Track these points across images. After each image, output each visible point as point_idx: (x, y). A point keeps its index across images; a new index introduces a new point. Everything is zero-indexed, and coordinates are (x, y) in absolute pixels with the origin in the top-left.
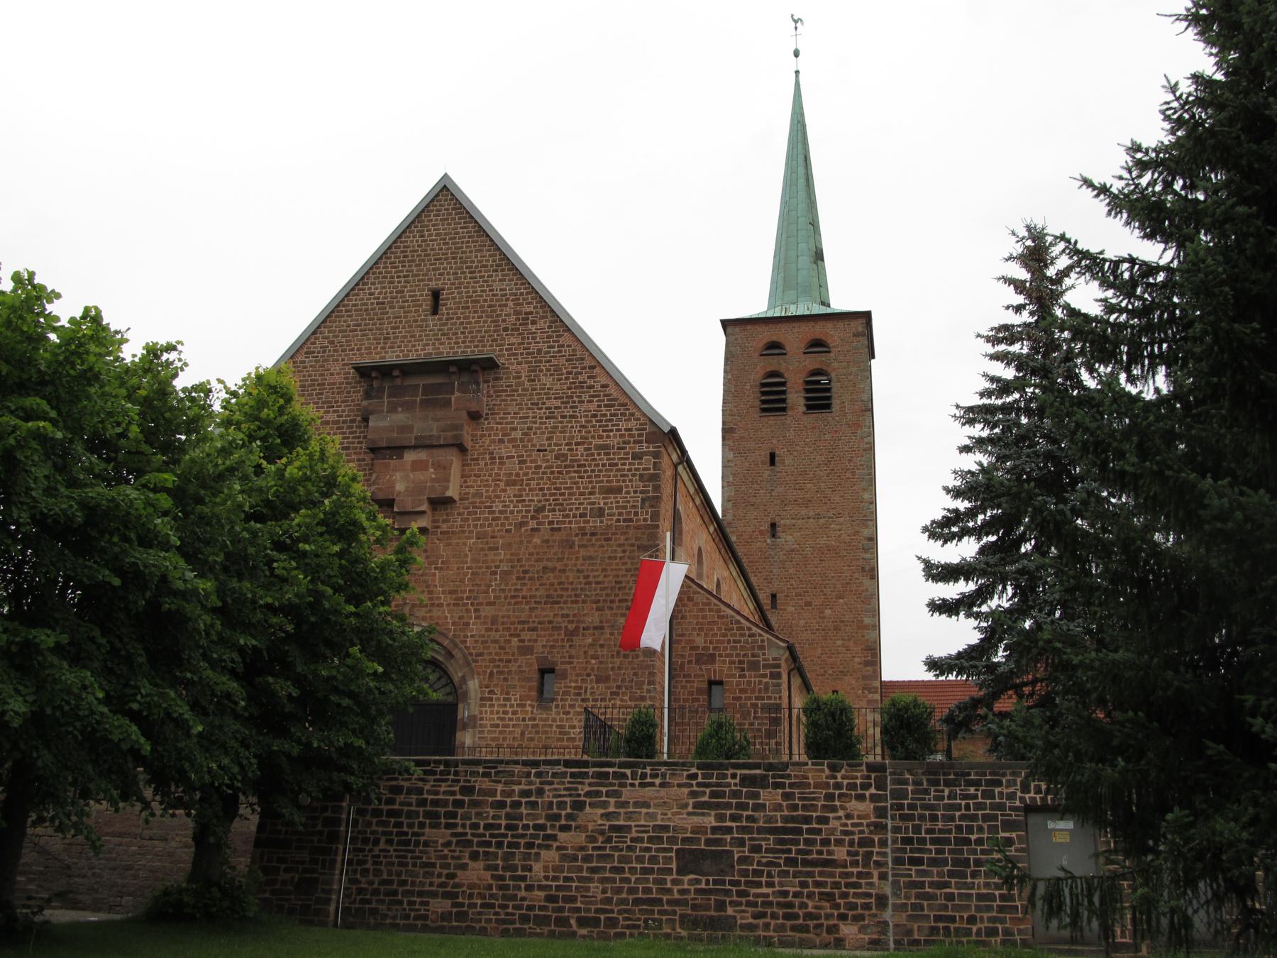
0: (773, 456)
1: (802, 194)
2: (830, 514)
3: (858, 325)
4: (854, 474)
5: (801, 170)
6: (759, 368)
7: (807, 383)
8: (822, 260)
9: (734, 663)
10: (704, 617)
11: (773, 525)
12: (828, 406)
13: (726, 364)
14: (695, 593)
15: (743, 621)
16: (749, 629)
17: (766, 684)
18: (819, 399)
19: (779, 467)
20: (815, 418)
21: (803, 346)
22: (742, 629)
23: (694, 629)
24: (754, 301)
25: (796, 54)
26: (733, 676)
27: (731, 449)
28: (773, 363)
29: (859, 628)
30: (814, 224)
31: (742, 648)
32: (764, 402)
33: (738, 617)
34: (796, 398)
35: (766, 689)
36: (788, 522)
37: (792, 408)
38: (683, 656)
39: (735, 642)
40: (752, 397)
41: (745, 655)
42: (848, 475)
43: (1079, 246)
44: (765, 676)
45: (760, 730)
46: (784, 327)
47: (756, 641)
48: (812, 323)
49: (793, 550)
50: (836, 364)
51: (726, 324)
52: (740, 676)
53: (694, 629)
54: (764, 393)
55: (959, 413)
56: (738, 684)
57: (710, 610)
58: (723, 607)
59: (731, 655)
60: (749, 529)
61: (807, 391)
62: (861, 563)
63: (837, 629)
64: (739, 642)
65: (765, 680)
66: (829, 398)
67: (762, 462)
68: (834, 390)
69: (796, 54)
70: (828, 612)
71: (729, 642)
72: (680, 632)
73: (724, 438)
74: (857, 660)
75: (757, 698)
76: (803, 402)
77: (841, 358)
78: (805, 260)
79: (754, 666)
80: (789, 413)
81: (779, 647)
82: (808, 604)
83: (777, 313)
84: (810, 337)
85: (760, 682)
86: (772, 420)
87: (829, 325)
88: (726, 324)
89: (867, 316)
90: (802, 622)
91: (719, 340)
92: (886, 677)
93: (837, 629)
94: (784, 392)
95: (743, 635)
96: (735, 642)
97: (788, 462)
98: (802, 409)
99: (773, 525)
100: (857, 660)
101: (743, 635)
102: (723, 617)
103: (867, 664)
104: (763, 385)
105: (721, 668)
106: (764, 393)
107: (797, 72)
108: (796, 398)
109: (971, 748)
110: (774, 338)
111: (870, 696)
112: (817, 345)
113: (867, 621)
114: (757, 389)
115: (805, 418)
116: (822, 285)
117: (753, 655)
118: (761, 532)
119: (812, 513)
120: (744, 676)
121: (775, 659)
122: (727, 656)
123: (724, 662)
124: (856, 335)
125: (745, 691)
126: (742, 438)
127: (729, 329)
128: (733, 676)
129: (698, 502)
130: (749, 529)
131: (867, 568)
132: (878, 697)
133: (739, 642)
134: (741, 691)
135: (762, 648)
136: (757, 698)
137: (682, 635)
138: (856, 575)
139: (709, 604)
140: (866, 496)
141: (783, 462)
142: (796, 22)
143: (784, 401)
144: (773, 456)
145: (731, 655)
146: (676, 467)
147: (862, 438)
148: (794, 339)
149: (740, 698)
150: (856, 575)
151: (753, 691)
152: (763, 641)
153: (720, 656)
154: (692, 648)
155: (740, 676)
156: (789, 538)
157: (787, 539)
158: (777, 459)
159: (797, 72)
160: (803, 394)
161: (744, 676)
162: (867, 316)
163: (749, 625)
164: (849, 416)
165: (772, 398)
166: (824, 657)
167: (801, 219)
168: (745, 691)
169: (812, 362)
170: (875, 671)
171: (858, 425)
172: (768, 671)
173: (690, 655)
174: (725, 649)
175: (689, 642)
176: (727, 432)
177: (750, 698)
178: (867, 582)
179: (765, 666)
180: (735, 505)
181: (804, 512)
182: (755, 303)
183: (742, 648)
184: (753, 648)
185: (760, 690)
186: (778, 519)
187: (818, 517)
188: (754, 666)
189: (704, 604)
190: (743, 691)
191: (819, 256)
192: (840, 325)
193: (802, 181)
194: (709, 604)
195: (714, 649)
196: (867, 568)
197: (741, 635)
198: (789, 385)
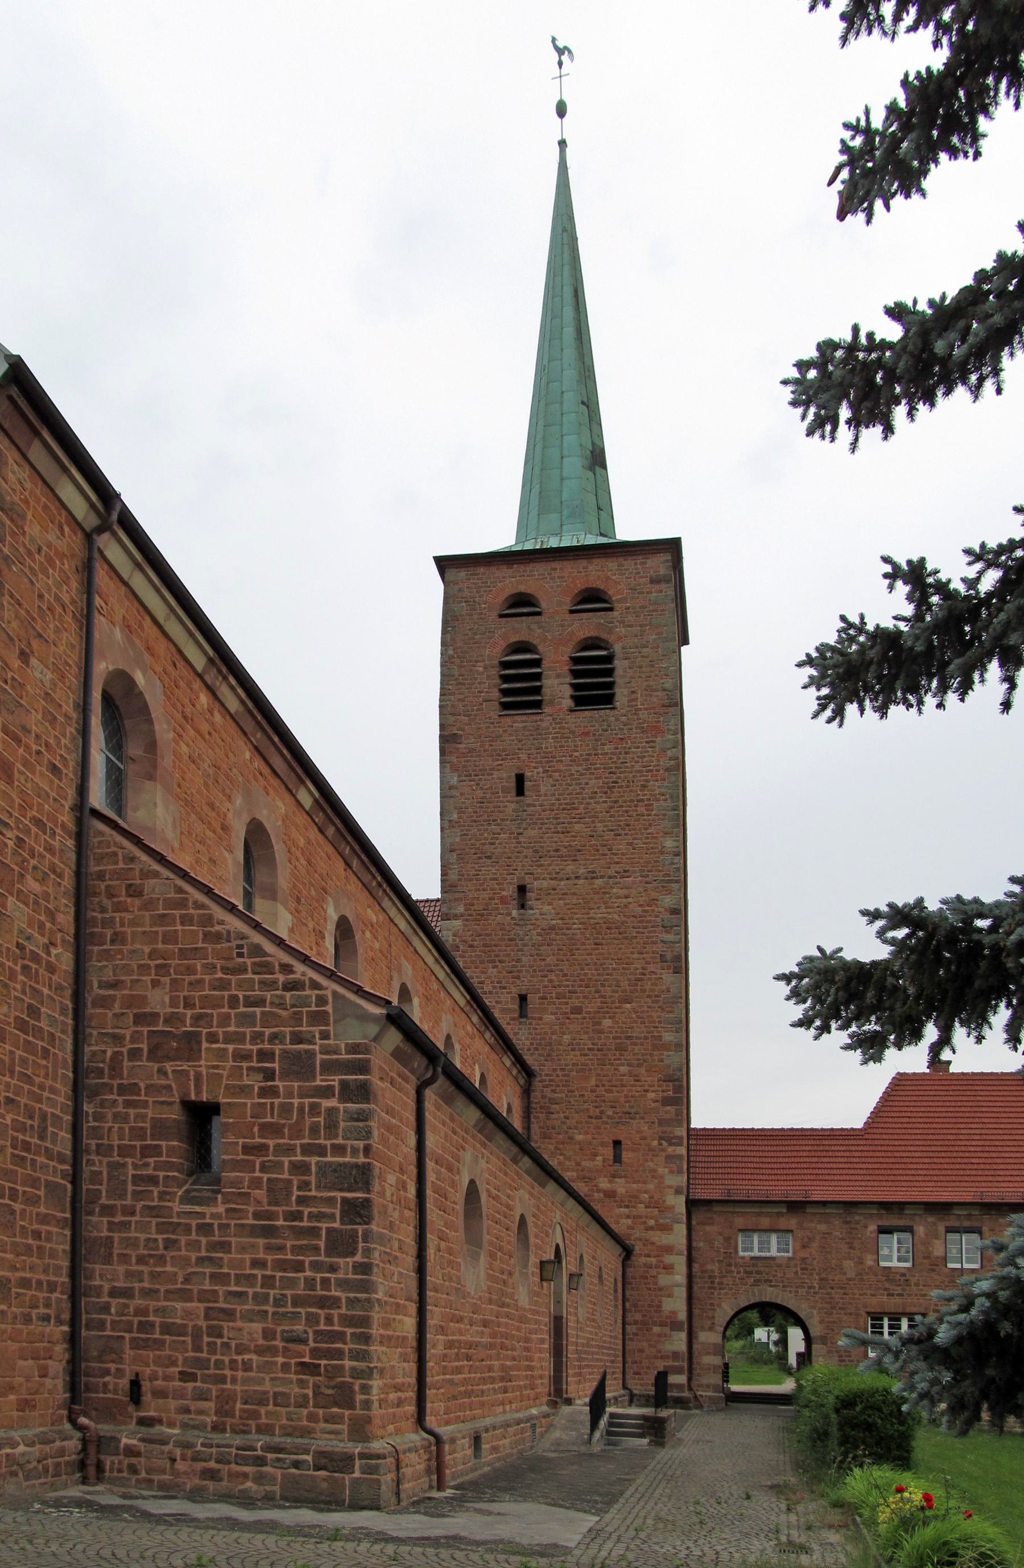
0: (520, 779)
1: (570, 353)
2: (610, 872)
3: (659, 564)
4: (649, 807)
5: (569, 312)
6: (498, 637)
7: (576, 661)
8: (604, 466)
9: (246, 1057)
10: (170, 938)
11: (522, 889)
12: (608, 700)
13: (444, 632)
14: (147, 874)
15: (269, 947)
16: (286, 968)
17: (331, 1112)
18: (594, 683)
19: (530, 796)
20: (591, 717)
21: (568, 600)
22: (265, 967)
23: (144, 969)
24: (494, 526)
25: (561, 110)
26: (244, 1090)
27: (455, 769)
28: (521, 629)
29: (655, 1047)
30: (590, 406)
31: (267, 1019)
32: (505, 692)
33: (257, 938)
34: (557, 686)
35: (331, 1127)
36: (545, 884)
37: (551, 703)
38: (117, 1039)
39: (249, 1002)
40: (488, 685)
41: (274, 1037)
42: (641, 809)
43: (992, 544)
44: (326, 1092)
45: (314, 1232)
46: (539, 569)
47: (305, 1002)
48: (583, 563)
49: (552, 928)
50: (620, 631)
51: (443, 563)
52: (264, 1092)
53: (144, 969)
54: (505, 679)
55: (785, 989)
56: (259, 1111)
57: (186, 920)
58: (218, 912)
59: (240, 1038)
60: (485, 895)
61: (576, 674)
62: (659, 948)
63: (621, 1048)
64: (260, 1002)
65: (327, 1103)
66: (610, 685)
67: (505, 790)
68: (619, 672)
69: (561, 110)
70: (607, 1023)
71: (234, 1002)
72: (109, 975)
73: (443, 752)
74: (651, 1095)
75: (307, 1150)
76: (568, 691)
77: (630, 618)
78: (574, 464)
79: (300, 1066)
80: (547, 710)
81: (364, 1017)
82: (577, 1010)
83: (529, 546)
84: (580, 585)
85: (314, 1109)
86: (520, 721)
87: (612, 564)
88: (443, 563)
89: (672, 547)
90: (567, 1038)
91: (433, 589)
92: (697, 1122)
93: (621, 1048)
94: (538, 677)
95: (272, 985)
96: (249, 1002)
97: (543, 787)
98: (568, 703)
99: (522, 889)
100: (651, 1095)
101: (272, 985)
102: (217, 937)
103: (666, 1102)
104: (505, 665)
105: (211, 1074)
106: (505, 679)
107: (562, 144)
108: (557, 686)
109: (822, 1227)
110: (522, 588)
111: (670, 1149)
112: (592, 599)
113: (668, 1037)
114: (495, 672)
115: (571, 718)
116: (603, 507)
117: (297, 1038)
118: (503, 900)
119: (581, 871)
120: (273, 1092)
121: (354, 1049)
122: (228, 1039)
123: (222, 1054)
124: (654, 581)
125: (275, 1130)
126: (471, 751)
127: (451, 574)
128: (244, 1090)
129: (233, 704)
130: (485, 895)
131: (669, 956)
132: (682, 1151)
133: (260, 1002)
134: (269, 1130)
135: (319, 1018)
136: (307, 1150)
137: (115, 985)
138: (651, 968)
139: (182, 904)
140: (669, 843)
141: (536, 788)
142: (560, 51)
143: (538, 690)
144: (520, 779)
145: (240, 1038)
146: (89, 537)
147: (664, 751)
148: (553, 587)
149: (262, 1149)
150: (651, 968)
151: (297, 1132)
152: (322, 1001)
153: (212, 1038)
154: (140, 1019)
155: (264, 1092)
156: (547, 908)
157: (542, 910)
158: (527, 784)
159: (562, 144)
160: (569, 679)
161: (273, 1092)
162: (672, 547)
163: (287, 959)
164: (643, 715)
165: (519, 686)
166: (600, 1090)
167: (566, 396)
168: (275, 1130)
169: (586, 626)
170: (678, 1113)
171: (656, 729)
172: (335, 1080)
173: (136, 1037)
174: (225, 1020)
175: (130, 1002)
176: (448, 740)
177: (290, 1150)
178: (669, 978)
179: (328, 1067)
180: (460, 858)
181: (570, 868)
182: (497, 531)
183: (267, 1019)
184: (297, 1018)
185: (315, 1130)
186: (528, 879)
187: (592, 876)
188: (300, 1066)
189: (170, 904)
190: (272, 1130)
191: (597, 459)
192: (629, 564)
193: (569, 332)
194: (182, 904)
195: (197, 1019)
196: (669, 956)
197: (265, 985)
198: (545, 664)
